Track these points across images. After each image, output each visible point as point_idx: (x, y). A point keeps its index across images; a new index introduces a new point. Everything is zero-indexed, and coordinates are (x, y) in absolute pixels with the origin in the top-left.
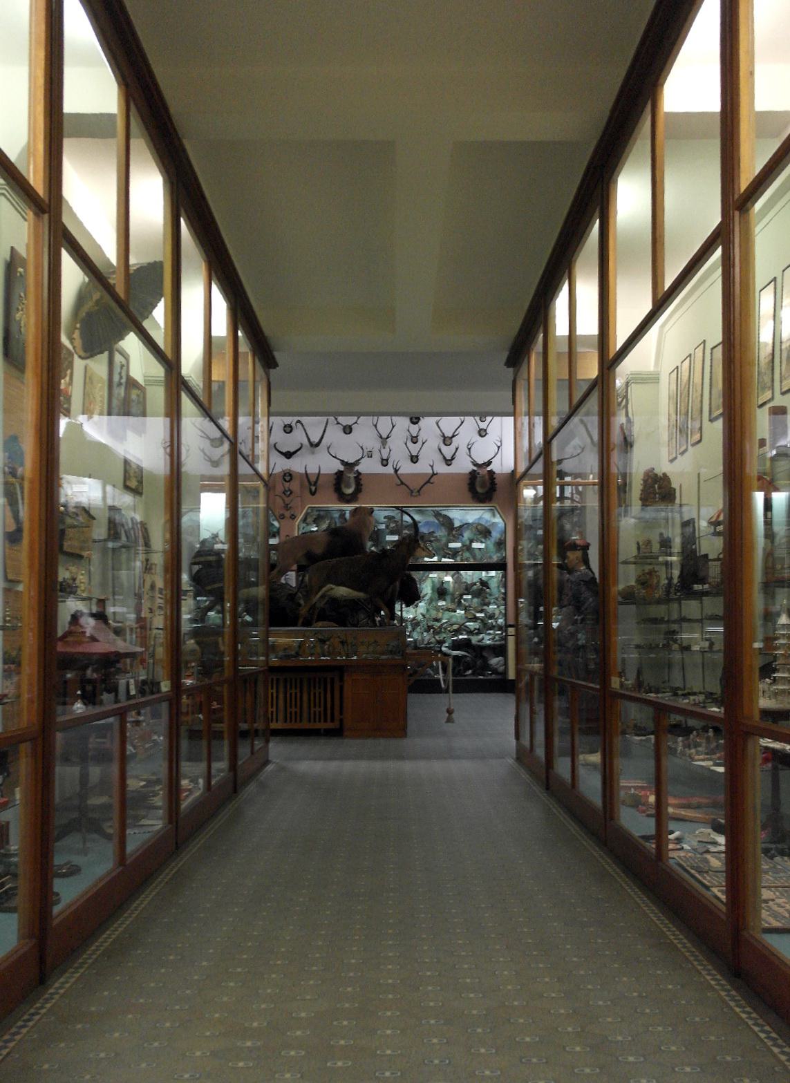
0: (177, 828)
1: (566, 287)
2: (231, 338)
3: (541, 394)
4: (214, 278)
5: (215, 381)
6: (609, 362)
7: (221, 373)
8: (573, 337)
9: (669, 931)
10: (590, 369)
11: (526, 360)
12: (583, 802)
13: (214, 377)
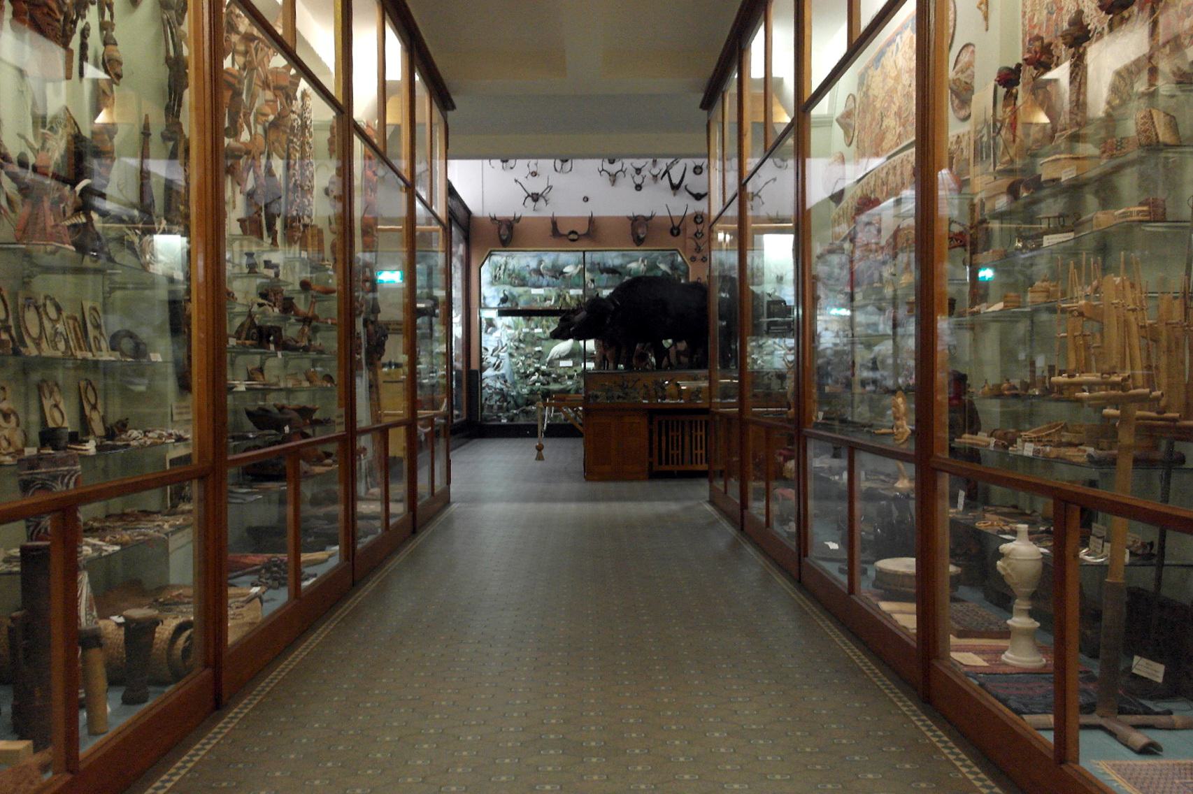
0: (353, 564)
1: (761, 31)
2: (406, 82)
3: (735, 136)
4: (387, 17)
5: (389, 125)
6: (804, 104)
7: (396, 114)
8: (769, 80)
9: (884, 684)
10: (783, 117)
11: (720, 98)
12: (825, 581)
13: (389, 121)
